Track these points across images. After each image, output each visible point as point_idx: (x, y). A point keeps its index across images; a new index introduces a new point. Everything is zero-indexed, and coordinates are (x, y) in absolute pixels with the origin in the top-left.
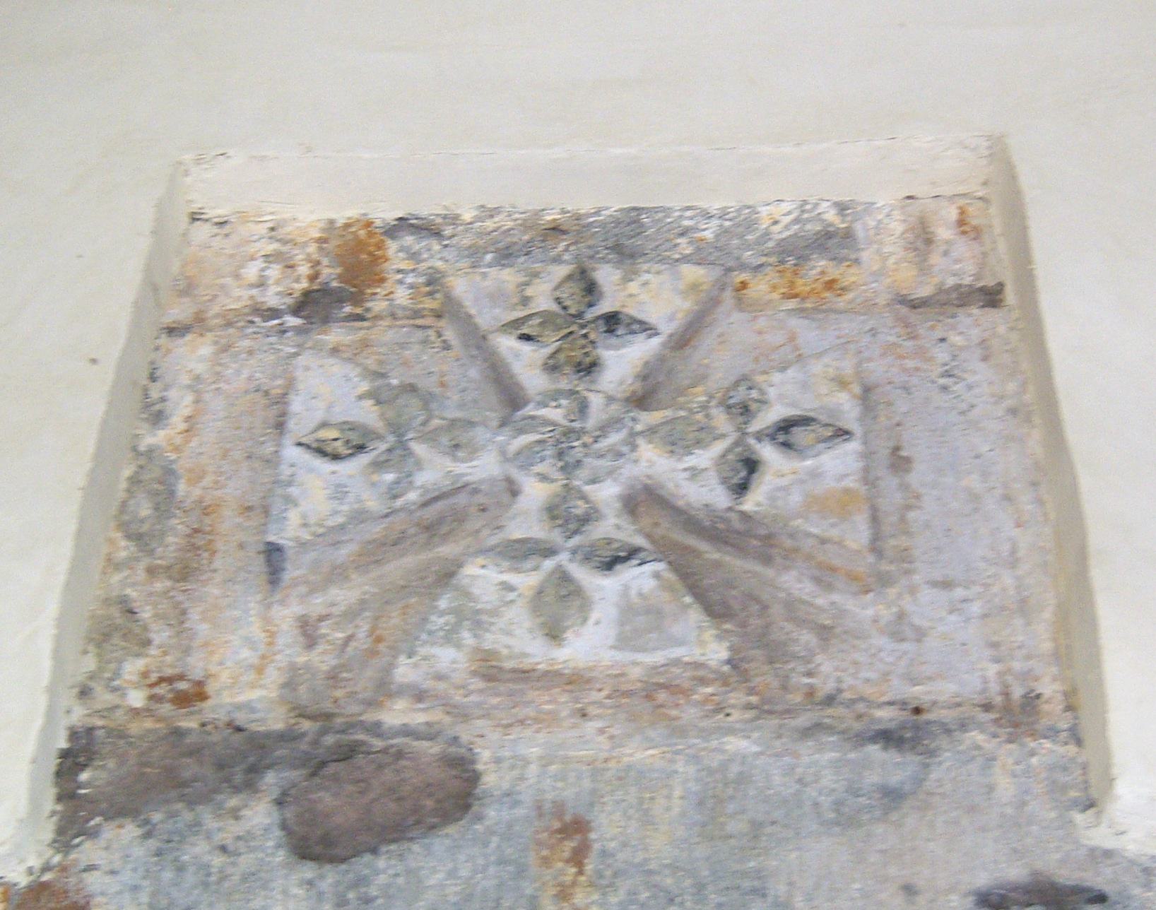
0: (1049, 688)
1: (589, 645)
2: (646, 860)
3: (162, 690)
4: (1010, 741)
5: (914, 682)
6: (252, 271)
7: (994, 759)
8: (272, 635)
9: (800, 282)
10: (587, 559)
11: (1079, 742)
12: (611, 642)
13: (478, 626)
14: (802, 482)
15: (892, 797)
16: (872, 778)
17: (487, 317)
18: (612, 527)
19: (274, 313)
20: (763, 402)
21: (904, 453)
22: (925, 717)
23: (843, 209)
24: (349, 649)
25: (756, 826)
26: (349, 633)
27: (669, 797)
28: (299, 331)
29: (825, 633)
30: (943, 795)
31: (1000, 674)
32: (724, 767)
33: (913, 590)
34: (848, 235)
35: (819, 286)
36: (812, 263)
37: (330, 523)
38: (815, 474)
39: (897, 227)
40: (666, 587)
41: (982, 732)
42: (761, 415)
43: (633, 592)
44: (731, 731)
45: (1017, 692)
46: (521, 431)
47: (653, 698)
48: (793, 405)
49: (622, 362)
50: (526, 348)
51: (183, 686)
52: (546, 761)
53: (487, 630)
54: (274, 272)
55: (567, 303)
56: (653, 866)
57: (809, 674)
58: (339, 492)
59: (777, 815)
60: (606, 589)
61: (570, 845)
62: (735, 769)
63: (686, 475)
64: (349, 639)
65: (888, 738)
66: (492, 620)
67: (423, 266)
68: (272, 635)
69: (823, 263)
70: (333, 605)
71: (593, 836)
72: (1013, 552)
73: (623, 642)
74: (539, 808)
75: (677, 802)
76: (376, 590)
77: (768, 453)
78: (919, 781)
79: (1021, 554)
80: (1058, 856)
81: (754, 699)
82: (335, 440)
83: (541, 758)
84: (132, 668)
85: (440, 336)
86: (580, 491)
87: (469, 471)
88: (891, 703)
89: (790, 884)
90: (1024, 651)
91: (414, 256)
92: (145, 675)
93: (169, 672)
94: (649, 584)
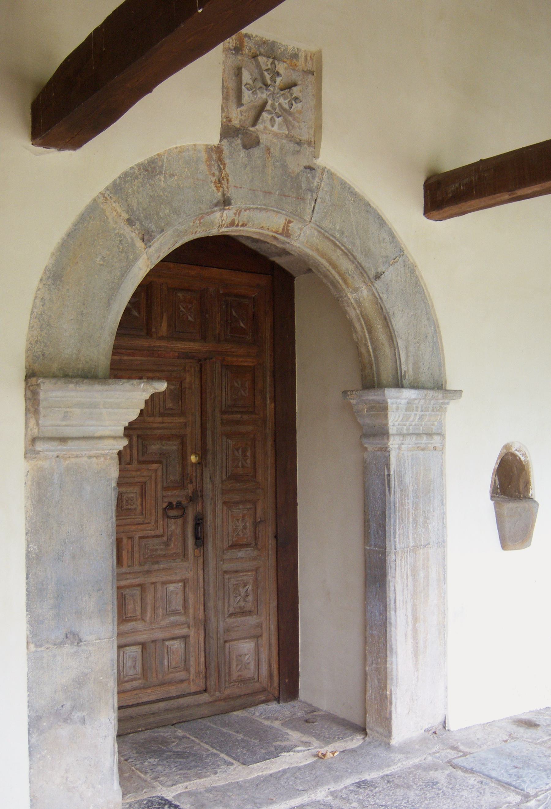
1: (275, 128)
15: (298, 152)
16: (296, 149)
17: (264, 67)
19: (231, 50)
29: (293, 126)
73: (278, 129)
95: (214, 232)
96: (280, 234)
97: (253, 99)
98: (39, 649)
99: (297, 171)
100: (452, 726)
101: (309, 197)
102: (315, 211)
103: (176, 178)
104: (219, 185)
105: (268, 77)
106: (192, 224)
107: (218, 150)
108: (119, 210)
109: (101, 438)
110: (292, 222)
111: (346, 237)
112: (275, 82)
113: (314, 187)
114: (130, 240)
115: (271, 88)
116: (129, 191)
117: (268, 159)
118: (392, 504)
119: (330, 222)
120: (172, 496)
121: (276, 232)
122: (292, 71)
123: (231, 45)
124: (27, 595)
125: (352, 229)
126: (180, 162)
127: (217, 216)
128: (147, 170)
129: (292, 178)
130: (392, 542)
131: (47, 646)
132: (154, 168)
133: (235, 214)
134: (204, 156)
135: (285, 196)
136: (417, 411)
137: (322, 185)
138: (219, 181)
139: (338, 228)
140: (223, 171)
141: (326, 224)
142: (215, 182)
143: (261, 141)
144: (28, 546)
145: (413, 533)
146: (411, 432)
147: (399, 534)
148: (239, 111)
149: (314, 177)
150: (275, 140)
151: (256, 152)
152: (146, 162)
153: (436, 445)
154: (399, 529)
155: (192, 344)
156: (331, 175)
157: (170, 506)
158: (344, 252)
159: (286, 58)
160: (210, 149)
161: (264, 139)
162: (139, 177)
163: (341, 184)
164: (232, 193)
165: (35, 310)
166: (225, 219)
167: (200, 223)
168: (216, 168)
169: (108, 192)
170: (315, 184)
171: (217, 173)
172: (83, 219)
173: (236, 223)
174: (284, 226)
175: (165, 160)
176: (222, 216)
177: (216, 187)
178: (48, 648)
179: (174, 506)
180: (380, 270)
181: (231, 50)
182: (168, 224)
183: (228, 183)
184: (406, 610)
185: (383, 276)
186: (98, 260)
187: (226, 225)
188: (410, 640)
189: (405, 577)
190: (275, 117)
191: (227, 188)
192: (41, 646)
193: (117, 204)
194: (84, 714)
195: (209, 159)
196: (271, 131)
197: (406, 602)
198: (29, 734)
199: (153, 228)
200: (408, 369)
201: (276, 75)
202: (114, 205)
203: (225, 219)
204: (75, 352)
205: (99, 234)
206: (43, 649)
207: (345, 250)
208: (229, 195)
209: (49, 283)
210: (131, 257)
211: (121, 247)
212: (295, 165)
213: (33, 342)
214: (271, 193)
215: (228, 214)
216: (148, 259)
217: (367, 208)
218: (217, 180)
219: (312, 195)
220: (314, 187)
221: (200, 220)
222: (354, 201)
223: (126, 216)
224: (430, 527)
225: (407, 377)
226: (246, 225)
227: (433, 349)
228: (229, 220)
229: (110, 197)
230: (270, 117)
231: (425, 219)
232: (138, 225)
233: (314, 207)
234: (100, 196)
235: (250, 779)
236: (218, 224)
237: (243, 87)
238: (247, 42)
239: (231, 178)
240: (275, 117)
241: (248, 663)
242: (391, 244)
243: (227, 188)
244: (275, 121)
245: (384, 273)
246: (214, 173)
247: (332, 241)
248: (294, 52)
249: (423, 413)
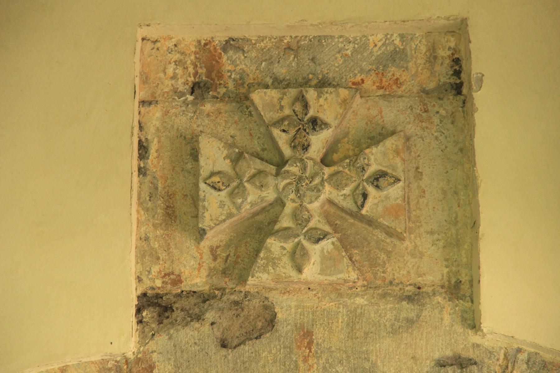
0: (464, 278)
1: (311, 271)
2: (331, 347)
3: (166, 279)
4: (449, 301)
5: (420, 276)
6: (170, 70)
7: (444, 308)
8: (201, 254)
9: (384, 80)
10: (309, 239)
11: (472, 301)
12: (319, 272)
13: (274, 265)
14: (382, 201)
15: (410, 322)
16: (404, 315)
18: (316, 222)
19: (182, 94)
20: (368, 165)
21: (420, 170)
22: (421, 290)
23: (402, 38)
24: (228, 261)
25: (366, 334)
26: (228, 253)
27: (338, 322)
28: (194, 103)
30: (426, 322)
31: (448, 272)
32: (356, 309)
33: (420, 236)
35: (391, 82)
36: (389, 69)
37: (220, 219)
38: (387, 197)
39: (423, 49)
40: (336, 248)
41: (441, 297)
42: (368, 169)
43: (325, 251)
44: (357, 295)
45: (453, 281)
46: (285, 178)
48: (380, 164)
49: (318, 142)
50: (283, 134)
51: (172, 277)
52: (297, 307)
53: (277, 266)
54: (179, 71)
55: (298, 113)
56: (333, 349)
57: (384, 272)
58: (222, 205)
59: (373, 329)
60: (316, 251)
61: (306, 341)
62: (359, 311)
63: (342, 198)
64: (228, 256)
65: (409, 299)
66: (279, 262)
67: (238, 68)
68: (201, 254)
69: (393, 69)
70: (221, 241)
71: (314, 337)
72: (456, 218)
73: (322, 272)
74: (296, 326)
75: (340, 324)
76: (235, 235)
77: (371, 190)
78: (418, 316)
79: (458, 219)
80: (462, 347)
81: (365, 283)
82: (219, 182)
83: (295, 306)
84: (155, 269)
85: (247, 109)
86: (306, 208)
87: (267, 195)
88: (410, 285)
89: (377, 356)
90: (457, 263)
91: (233, 62)
92: (160, 272)
93: (167, 271)
94: (331, 247)
97: (234, 211)
115: (294, 169)
117: (305, 360)
122: (382, 103)
123: (181, 81)
150: (327, 304)
161: (287, 309)
190: (305, 243)
196: (299, 282)
230: (289, 245)
237: (202, 186)
240: (305, 243)
248: (390, 48)
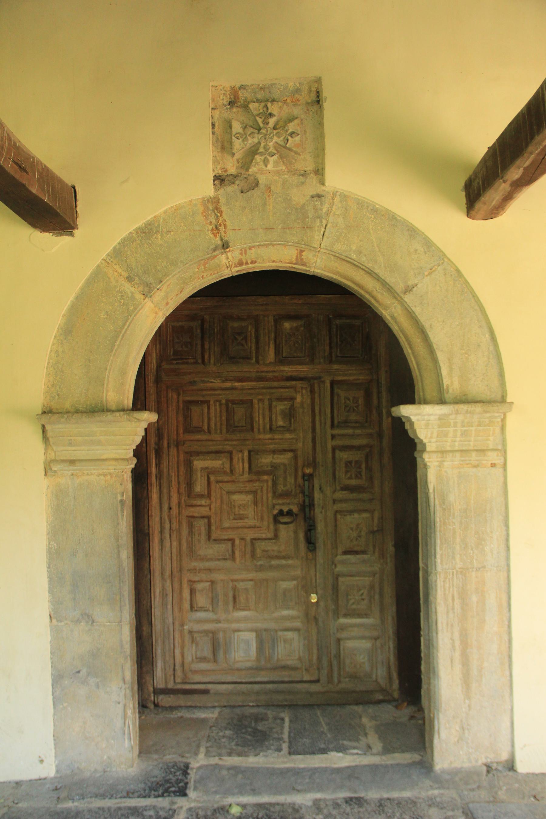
1: (270, 167)
15: (303, 183)
16: (300, 181)
17: (255, 113)
18: (272, 150)
19: (225, 106)
25: (288, 187)
29: (296, 160)
34: (300, 89)
38: (295, 141)
47: (278, 173)
49: (272, 121)
60: (271, 159)
65: (302, 175)
77: (289, 138)
84: (219, 167)
95: (227, 273)
96: (295, 264)
98: (60, 624)
99: (302, 202)
100: (522, 767)
101: (318, 225)
102: (325, 237)
103: (172, 233)
104: (217, 231)
105: (260, 121)
106: (196, 270)
107: (215, 201)
108: (120, 271)
109: (106, 460)
110: (304, 251)
111: (365, 256)
112: (268, 124)
113: (323, 213)
114: (130, 294)
115: (263, 131)
116: (128, 253)
117: (269, 196)
118: (432, 524)
119: (344, 244)
120: (283, 504)
121: (291, 263)
124: (49, 581)
125: (373, 246)
126: (177, 219)
127: (223, 259)
128: (144, 232)
129: (296, 209)
130: (433, 562)
131: (66, 622)
132: (151, 229)
133: (241, 254)
134: (201, 209)
135: (289, 228)
136: (455, 426)
137: (333, 209)
138: (216, 227)
139: (354, 248)
140: (220, 218)
141: (339, 247)
142: (212, 230)
143: (260, 182)
144: (49, 543)
145: (461, 555)
146: (457, 448)
147: (442, 555)
148: (235, 160)
149: (322, 204)
150: (276, 178)
151: (256, 193)
152: (144, 225)
153: (493, 462)
154: (441, 549)
155: (299, 367)
156: (344, 197)
157: (281, 513)
158: (366, 271)
159: (286, 96)
160: (206, 202)
161: (262, 180)
162: (137, 239)
163: (358, 204)
164: (230, 236)
165: (51, 361)
166: (232, 260)
167: (205, 268)
168: (213, 217)
169: (109, 258)
170: (325, 210)
171: (214, 221)
172: (89, 283)
173: (244, 262)
174: (297, 257)
175: (161, 220)
176: (228, 258)
177: (213, 234)
178: (66, 624)
179: (285, 513)
180: (410, 283)
181: (225, 106)
182: (166, 275)
183: (225, 228)
184: (452, 633)
185: (415, 289)
186: (102, 314)
187: (233, 265)
188: (458, 667)
189: (450, 600)
190: (268, 157)
191: (225, 232)
192: (61, 622)
193: (118, 266)
194: (98, 680)
195: (206, 208)
197: (452, 625)
198: (53, 688)
199: (151, 280)
200: (452, 382)
201: (269, 116)
202: (115, 267)
203: (232, 260)
204: (84, 391)
205: (102, 293)
206: (62, 624)
207: (366, 269)
208: (226, 239)
209: (62, 338)
210: (131, 309)
211: (122, 301)
212: (300, 196)
213: (50, 386)
214: (274, 228)
215: (233, 255)
216: (155, 307)
217: (393, 221)
218: (214, 227)
219: (321, 222)
220: (323, 213)
221: (204, 265)
222: (374, 218)
223: (125, 274)
224: (487, 549)
225: (450, 391)
226: (256, 262)
227: (489, 358)
228: (236, 261)
229: (112, 261)
230: (263, 158)
231: (470, 220)
232: (137, 280)
233: (324, 232)
234: (103, 262)
235: (278, 769)
236: (226, 266)
237: (233, 138)
238: (243, 94)
239: (228, 223)
240: (268, 157)
241: (364, 663)
242: (426, 253)
243: (225, 232)
244: (268, 161)
245: (416, 285)
246: (211, 222)
247: (350, 263)
248: (296, 88)
249: (465, 428)
